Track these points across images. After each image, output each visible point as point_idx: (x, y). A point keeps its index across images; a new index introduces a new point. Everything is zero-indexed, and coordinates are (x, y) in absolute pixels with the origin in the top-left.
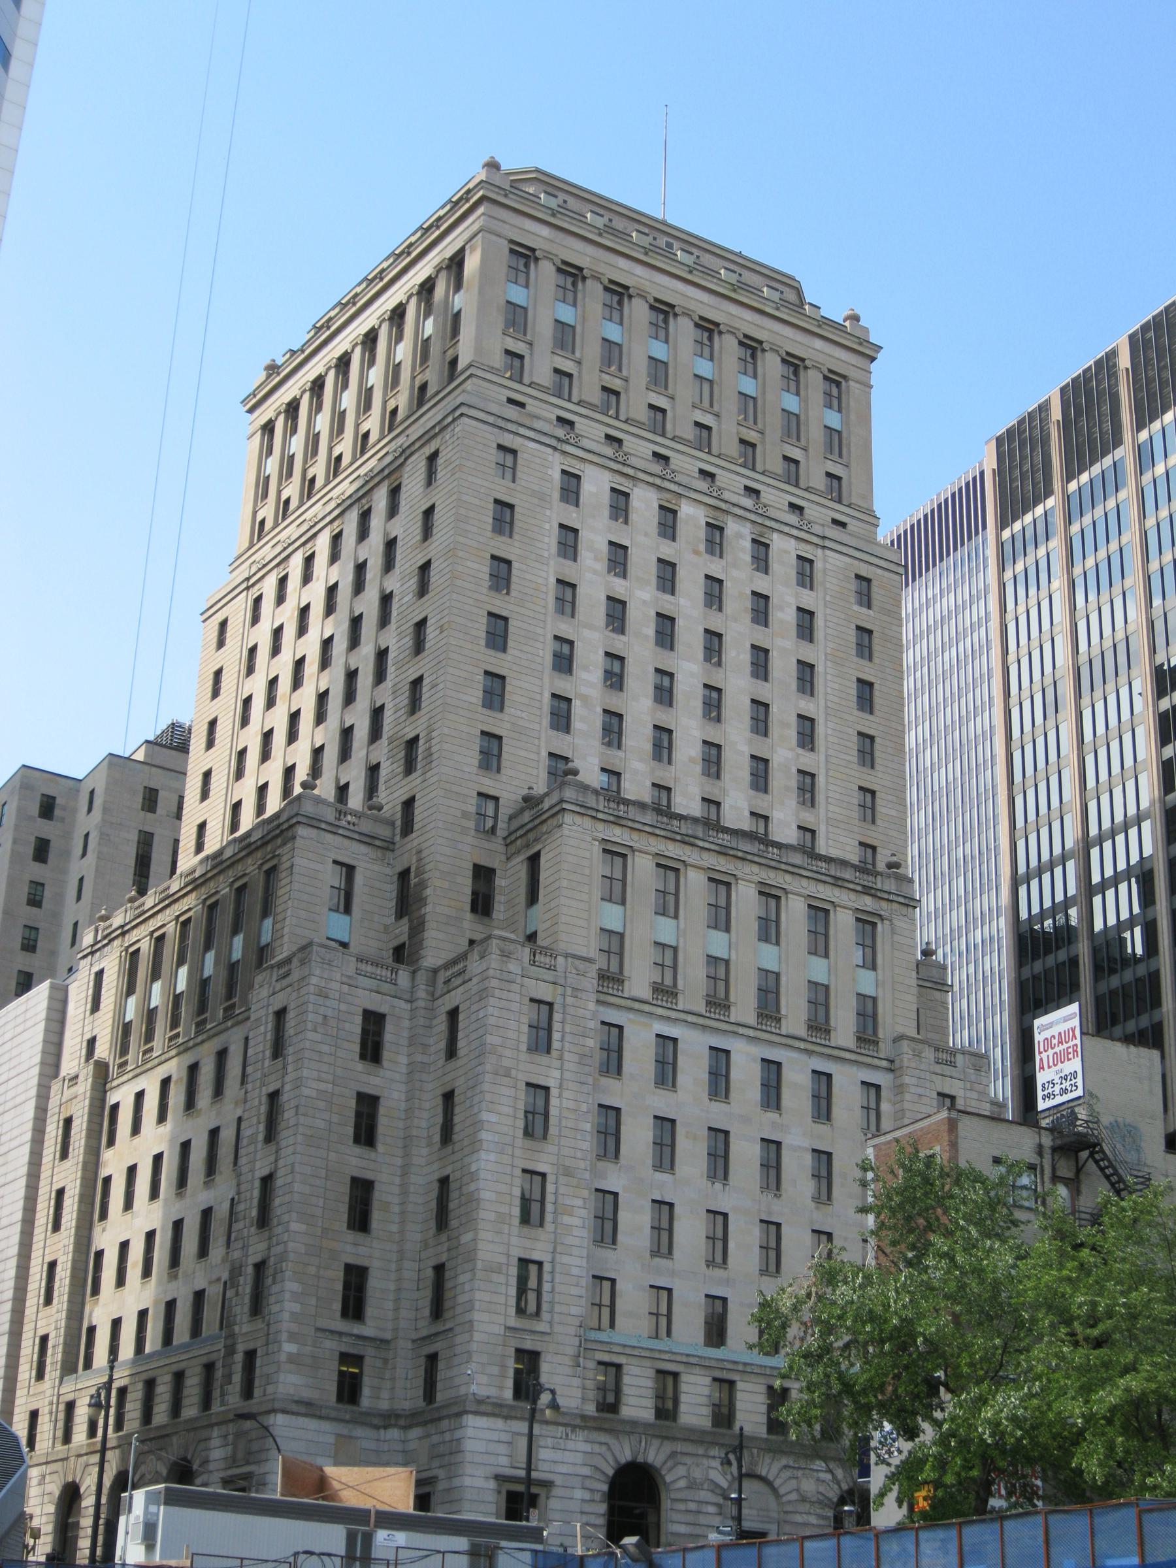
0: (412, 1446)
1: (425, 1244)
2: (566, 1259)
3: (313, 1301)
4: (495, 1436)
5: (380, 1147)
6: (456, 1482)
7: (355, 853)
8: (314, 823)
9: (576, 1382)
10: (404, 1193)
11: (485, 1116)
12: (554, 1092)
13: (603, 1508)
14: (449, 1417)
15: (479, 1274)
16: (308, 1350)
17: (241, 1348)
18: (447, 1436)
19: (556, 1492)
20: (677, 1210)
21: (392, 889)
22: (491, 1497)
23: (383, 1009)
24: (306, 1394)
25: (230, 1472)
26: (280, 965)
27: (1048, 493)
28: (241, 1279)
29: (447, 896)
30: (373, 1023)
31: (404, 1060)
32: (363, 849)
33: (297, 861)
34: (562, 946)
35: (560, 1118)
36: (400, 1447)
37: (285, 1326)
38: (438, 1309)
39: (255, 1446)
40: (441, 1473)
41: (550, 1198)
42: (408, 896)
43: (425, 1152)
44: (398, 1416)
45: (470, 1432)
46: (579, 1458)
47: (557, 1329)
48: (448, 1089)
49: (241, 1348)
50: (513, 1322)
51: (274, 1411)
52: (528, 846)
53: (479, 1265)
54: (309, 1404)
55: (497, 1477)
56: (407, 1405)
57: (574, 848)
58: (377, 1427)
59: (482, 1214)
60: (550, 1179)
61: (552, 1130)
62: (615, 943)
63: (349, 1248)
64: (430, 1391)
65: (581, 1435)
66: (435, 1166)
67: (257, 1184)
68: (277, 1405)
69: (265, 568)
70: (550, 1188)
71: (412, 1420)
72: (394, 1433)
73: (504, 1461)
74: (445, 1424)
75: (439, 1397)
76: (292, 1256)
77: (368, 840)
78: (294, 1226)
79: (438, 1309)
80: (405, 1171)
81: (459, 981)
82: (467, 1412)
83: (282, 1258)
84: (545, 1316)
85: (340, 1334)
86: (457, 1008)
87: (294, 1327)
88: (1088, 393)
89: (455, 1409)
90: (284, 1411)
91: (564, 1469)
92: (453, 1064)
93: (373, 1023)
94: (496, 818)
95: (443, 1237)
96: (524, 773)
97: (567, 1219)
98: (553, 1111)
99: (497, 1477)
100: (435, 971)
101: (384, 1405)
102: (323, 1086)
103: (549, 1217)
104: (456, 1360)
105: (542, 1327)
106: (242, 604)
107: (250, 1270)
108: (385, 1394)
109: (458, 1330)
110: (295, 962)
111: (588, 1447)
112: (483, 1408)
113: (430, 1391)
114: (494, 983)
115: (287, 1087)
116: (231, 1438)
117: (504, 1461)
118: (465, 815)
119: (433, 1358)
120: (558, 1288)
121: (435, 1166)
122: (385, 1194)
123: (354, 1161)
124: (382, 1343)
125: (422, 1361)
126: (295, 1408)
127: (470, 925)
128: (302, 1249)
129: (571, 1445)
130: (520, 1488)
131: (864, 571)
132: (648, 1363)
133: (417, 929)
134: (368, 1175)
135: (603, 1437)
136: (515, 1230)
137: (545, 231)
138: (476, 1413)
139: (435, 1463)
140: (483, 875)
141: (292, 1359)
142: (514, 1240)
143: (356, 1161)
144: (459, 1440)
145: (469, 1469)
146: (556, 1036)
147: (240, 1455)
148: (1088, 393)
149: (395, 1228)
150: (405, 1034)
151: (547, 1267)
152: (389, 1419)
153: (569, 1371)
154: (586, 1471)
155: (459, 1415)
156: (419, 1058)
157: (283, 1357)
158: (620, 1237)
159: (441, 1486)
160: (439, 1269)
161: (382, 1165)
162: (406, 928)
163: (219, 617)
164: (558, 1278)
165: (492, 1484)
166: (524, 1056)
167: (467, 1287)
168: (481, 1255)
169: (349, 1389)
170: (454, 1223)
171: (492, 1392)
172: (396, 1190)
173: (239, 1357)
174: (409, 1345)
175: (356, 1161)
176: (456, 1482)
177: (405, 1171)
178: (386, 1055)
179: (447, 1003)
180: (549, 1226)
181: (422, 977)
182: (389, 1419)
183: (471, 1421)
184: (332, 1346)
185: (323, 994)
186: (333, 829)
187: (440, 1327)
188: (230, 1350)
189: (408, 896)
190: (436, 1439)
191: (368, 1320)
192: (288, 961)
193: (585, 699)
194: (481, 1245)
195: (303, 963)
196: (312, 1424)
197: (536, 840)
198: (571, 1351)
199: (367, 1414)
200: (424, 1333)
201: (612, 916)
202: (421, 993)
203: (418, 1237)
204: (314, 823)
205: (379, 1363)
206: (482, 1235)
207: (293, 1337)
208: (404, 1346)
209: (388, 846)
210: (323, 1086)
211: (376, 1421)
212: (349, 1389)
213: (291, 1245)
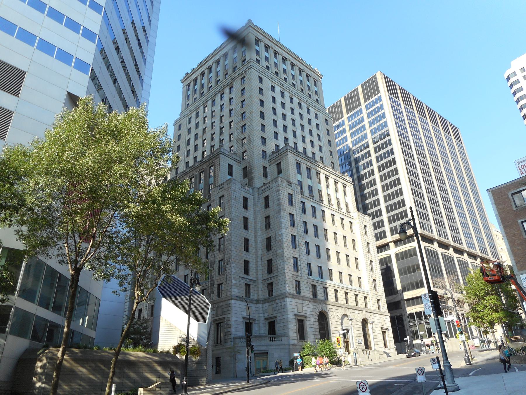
0: (265, 308)
1: (263, 255)
2: (303, 258)
3: (238, 269)
4: (293, 303)
5: (250, 231)
6: (284, 317)
7: (232, 163)
8: (224, 154)
9: (308, 289)
10: (256, 241)
11: (282, 220)
12: (295, 216)
13: (317, 323)
14: (280, 299)
15: (285, 260)
16: (238, 282)
17: (216, 284)
18: (280, 304)
19: (308, 319)
20: (320, 247)
21: (241, 173)
22: (294, 321)
23: (247, 197)
24: (239, 295)
25: (215, 318)
26: (219, 186)
27: (342, 117)
28: (215, 265)
29: (258, 173)
30: (245, 199)
31: (253, 210)
32: (234, 162)
33: (221, 162)
34: (291, 180)
35: (297, 222)
36: (261, 309)
37: (232, 276)
38: (270, 270)
39: (225, 310)
40: (278, 315)
41: (297, 242)
42: (246, 173)
43: (260, 232)
44: (260, 300)
45: (288, 303)
46: (311, 310)
47: (303, 275)
48: (267, 215)
49: (216, 284)
50: (293, 273)
51: (231, 299)
52: (276, 161)
53: (285, 258)
54: (239, 297)
55: (295, 315)
56: (261, 298)
57: (291, 159)
58: (255, 304)
59: (284, 245)
60: (297, 237)
61: (296, 225)
62: (300, 183)
63: (245, 256)
64: (270, 291)
65: (311, 303)
66: (265, 235)
67: (218, 240)
68: (232, 297)
69: (192, 111)
70: (297, 239)
71: (265, 301)
72: (260, 305)
73: (296, 310)
74: (278, 301)
75: (274, 294)
76: (233, 257)
77: (235, 160)
78: (233, 249)
79: (270, 270)
80: (256, 237)
81: (268, 189)
82: (286, 297)
83: (230, 257)
84: (300, 272)
85: (245, 278)
86: (268, 196)
87: (234, 276)
88: (351, 97)
89: (282, 297)
90: (234, 299)
91: (308, 313)
92: (268, 209)
93: (245, 199)
94: (266, 156)
95: (270, 252)
96: (270, 147)
97: (302, 247)
98: (295, 221)
99: (295, 315)
100: (259, 188)
101: (256, 298)
102: (236, 214)
103: (297, 247)
104: (280, 283)
105: (299, 275)
106: (186, 120)
107: (217, 262)
108: (256, 295)
109: (279, 275)
110: (225, 184)
111: (312, 307)
112: (290, 296)
113: (270, 291)
114: (280, 188)
115: (226, 214)
116: (215, 309)
117: (296, 310)
118: (260, 154)
119: (270, 284)
120: (302, 265)
121: (265, 235)
122: (251, 243)
123: (244, 234)
124: (254, 281)
125: (267, 285)
126: (236, 298)
127: (264, 180)
128: (235, 255)
129: (309, 306)
130: (248, 321)
131: (327, 118)
132: (321, 285)
133: (251, 180)
134: (248, 238)
135: (315, 304)
136: (291, 249)
137: (262, 36)
138: (289, 297)
139: (276, 312)
140: (265, 168)
141: (235, 285)
142: (291, 252)
143: (244, 234)
144: (284, 305)
145: (289, 313)
146: (294, 202)
147: (219, 312)
148: (351, 97)
149: (254, 251)
150: (252, 203)
151: (299, 259)
152: (258, 301)
153: (306, 286)
154: (313, 313)
155: (283, 298)
156: (257, 209)
157: (233, 284)
158: (310, 253)
159: (278, 319)
160: (270, 261)
161: (250, 235)
162: (247, 180)
163: (179, 124)
164: (301, 262)
165: (294, 317)
166: (288, 206)
167: (282, 263)
168: (285, 255)
169: (248, 293)
170: (273, 248)
171: (291, 292)
172: (254, 242)
173: (216, 286)
174: (261, 281)
175: (244, 234)
176: (284, 317)
177: (256, 237)
178: (249, 208)
179: (265, 195)
180: (298, 249)
181: (256, 190)
182: (258, 301)
183: (288, 299)
184: (243, 282)
185: (234, 191)
186: (228, 156)
187: (272, 275)
188: (212, 285)
189: (246, 173)
190: (274, 306)
191: (251, 275)
192: (223, 184)
193: (280, 133)
194: (285, 253)
195: (228, 184)
196: (241, 303)
197: (279, 159)
198: (306, 281)
199: (252, 300)
200: (266, 278)
201: (299, 177)
202: (256, 194)
203: (260, 253)
204: (224, 154)
205: (254, 286)
206: (285, 250)
207: (235, 279)
208: (260, 281)
209: (239, 162)
210: (236, 214)
211: (255, 302)
212: (248, 293)
213: (233, 254)
